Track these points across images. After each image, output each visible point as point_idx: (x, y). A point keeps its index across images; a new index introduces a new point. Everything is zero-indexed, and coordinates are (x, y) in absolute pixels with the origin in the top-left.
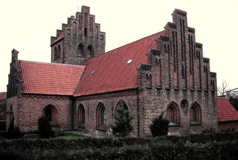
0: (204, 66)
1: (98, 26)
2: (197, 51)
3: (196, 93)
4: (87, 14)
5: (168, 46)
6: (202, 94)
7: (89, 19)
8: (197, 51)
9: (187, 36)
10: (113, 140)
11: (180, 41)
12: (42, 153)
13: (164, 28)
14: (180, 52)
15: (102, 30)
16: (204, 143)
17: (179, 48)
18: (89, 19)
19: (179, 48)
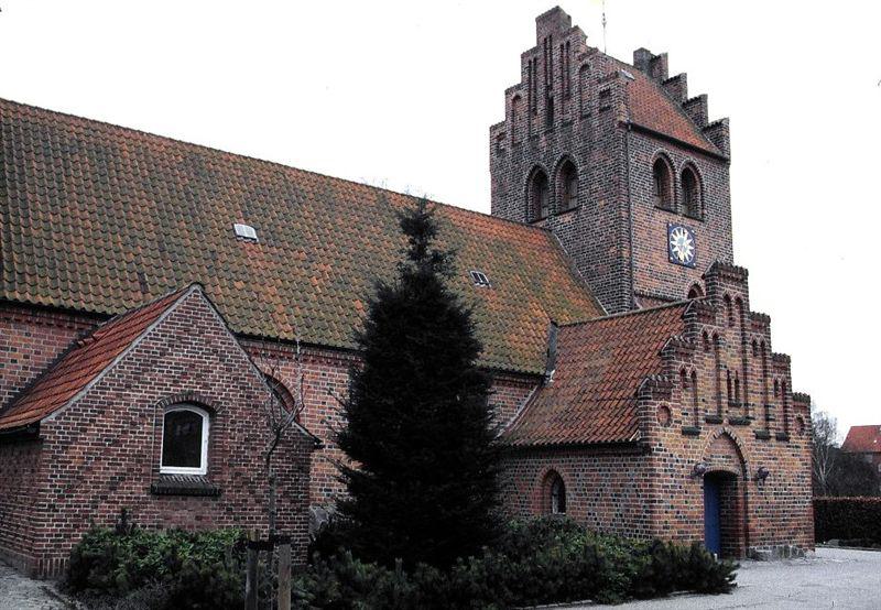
1: (513, 96)
15: (498, 114)
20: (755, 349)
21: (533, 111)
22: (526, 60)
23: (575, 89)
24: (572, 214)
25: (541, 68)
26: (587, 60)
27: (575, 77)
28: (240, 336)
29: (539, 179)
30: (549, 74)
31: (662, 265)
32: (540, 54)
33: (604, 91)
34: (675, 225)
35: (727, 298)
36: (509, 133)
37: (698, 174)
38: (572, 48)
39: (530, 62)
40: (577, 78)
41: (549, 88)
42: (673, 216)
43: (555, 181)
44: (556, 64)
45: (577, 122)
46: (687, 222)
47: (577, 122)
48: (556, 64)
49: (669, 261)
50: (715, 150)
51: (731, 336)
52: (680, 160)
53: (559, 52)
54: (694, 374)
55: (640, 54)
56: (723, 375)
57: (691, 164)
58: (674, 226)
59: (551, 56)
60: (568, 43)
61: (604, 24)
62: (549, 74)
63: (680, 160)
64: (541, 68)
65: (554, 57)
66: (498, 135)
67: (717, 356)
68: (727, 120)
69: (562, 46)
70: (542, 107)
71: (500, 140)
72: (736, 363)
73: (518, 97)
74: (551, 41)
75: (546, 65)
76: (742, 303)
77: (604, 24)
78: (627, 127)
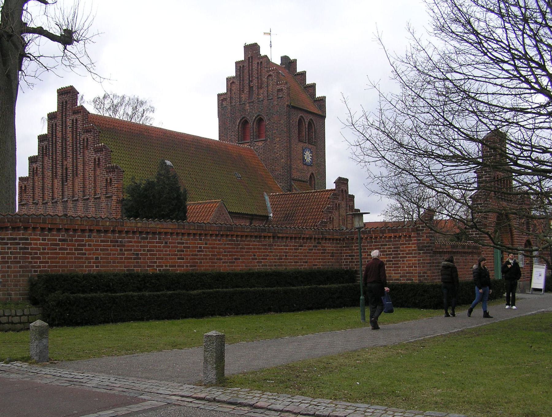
0: (95, 159)
1: (230, 81)
2: (84, 140)
3: (80, 204)
4: (252, 59)
5: (46, 147)
6: (90, 204)
7: (255, 66)
8: (84, 140)
9: (69, 123)
10: (510, 264)
11: (60, 133)
12: (359, 350)
13: (285, 59)
14: (59, 149)
15: (223, 90)
16: (111, 293)
17: (59, 144)
18: (255, 66)
19: (59, 144)
20: (350, 208)
21: (241, 91)
22: (238, 65)
23: (265, 85)
24: (263, 142)
25: (246, 71)
26: (271, 73)
27: (265, 79)
28: (229, 212)
29: (245, 123)
30: (250, 75)
31: (301, 166)
32: (246, 64)
33: (280, 89)
34: (306, 148)
35: (342, 190)
36: (229, 99)
37: (314, 124)
38: (263, 65)
39: (240, 67)
40: (266, 80)
41: (251, 81)
42: (305, 144)
43: (252, 124)
44: (255, 72)
45: (266, 101)
46: (310, 146)
47: (266, 101)
48: (255, 72)
49: (303, 164)
50: (316, 111)
51: (343, 204)
52: (307, 118)
53: (256, 65)
54: (333, 218)
55: (285, 59)
56: (341, 218)
57: (311, 120)
58: (305, 148)
59: (252, 67)
60: (261, 62)
61: (271, 47)
62: (250, 75)
63: (307, 118)
64: (246, 71)
65: (254, 67)
66: (221, 98)
67: (339, 211)
68: (325, 97)
69: (258, 63)
70: (247, 90)
71: (223, 101)
72: (344, 214)
73: (233, 82)
74: (252, 59)
75: (249, 70)
76: (347, 191)
77: (271, 47)
78: (290, 107)
